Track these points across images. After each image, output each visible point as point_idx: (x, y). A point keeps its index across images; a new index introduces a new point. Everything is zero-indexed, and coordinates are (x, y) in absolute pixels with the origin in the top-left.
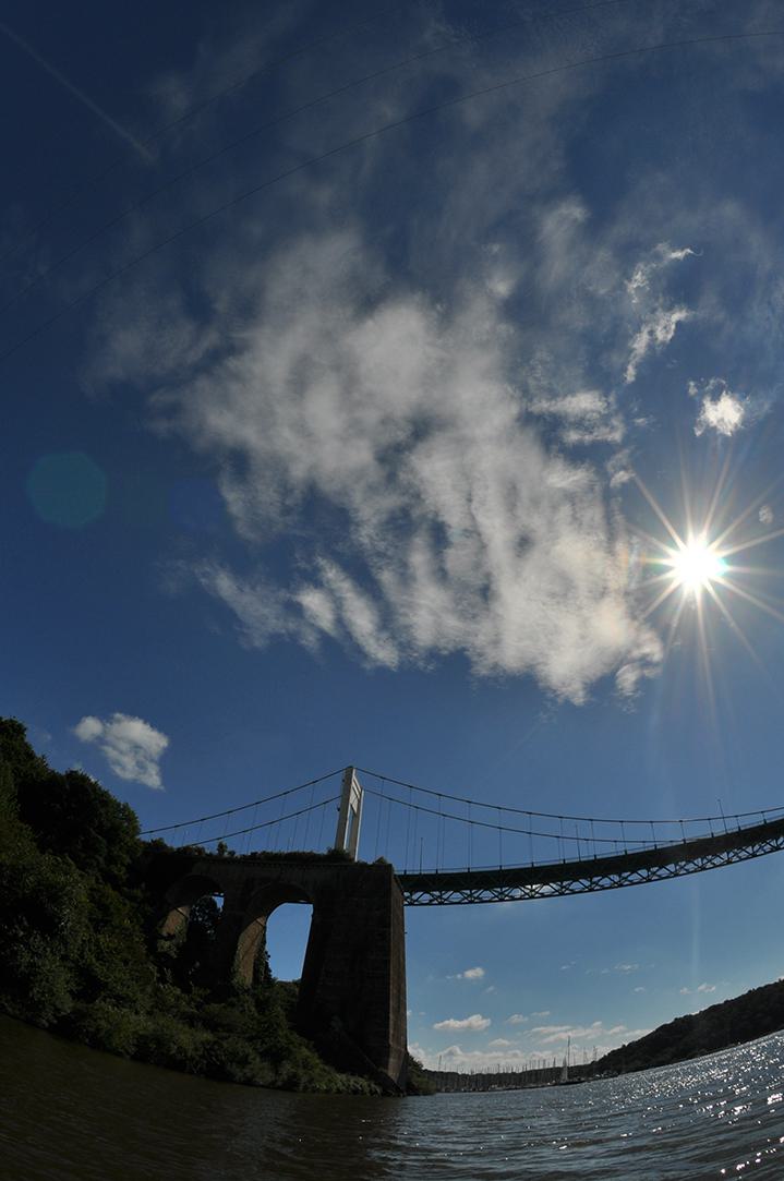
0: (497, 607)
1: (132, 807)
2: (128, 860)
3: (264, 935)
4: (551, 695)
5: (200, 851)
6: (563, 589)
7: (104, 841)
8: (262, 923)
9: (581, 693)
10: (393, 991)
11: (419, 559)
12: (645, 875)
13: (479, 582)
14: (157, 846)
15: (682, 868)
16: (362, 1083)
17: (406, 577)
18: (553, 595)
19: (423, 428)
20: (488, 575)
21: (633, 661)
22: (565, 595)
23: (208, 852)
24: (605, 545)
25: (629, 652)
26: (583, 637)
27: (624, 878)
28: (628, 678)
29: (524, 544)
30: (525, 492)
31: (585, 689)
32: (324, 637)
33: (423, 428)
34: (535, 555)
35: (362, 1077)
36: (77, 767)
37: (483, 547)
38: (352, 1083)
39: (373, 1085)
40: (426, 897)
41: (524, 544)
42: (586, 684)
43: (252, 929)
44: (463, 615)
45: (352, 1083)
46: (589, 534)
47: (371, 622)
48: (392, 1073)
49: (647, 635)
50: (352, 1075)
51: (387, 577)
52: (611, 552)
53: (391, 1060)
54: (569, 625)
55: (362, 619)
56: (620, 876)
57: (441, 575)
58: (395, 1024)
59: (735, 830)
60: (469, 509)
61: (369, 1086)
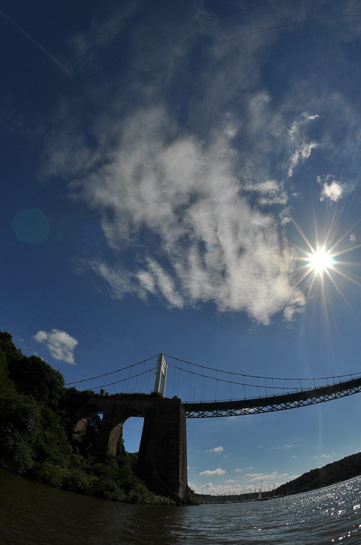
0: (229, 280)
1: (61, 373)
2: (59, 397)
3: (122, 432)
4: (254, 321)
5: (92, 393)
6: (259, 272)
7: (48, 388)
8: (121, 426)
9: (268, 320)
10: (181, 457)
11: (193, 258)
12: (297, 404)
13: (221, 269)
14: (72, 390)
15: (314, 400)
16: (167, 500)
17: (187, 266)
18: (254, 275)
19: (195, 197)
20: (225, 266)
21: (291, 305)
22: (260, 275)
23: (96, 393)
24: (279, 251)
25: (290, 301)
26: (268, 294)
27: (287, 405)
28: (289, 313)
29: (241, 251)
30: (242, 227)
31: (269, 318)
32: (149, 294)
33: (195, 197)
34: (246, 256)
35: (167, 497)
36: (36, 354)
37: (222, 253)
38: (162, 500)
39: (172, 501)
40: (196, 414)
41: (241, 251)
42: (270, 316)
43: (116, 429)
44: (213, 284)
45: (162, 500)
46: (271, 246)
47: (171, 287)
48: (181, 495)
49: (298, 293)
50: (162, 496)
51: (178, 266)
52: (281, 255)
53: (180, 489)
54: (262, 289)
55: (167, 286)
56: (285, 404)
57: (203, 265)
58: (182, 472)
59: (338, 383)
60: (216, 235)
61: (170, 501)
